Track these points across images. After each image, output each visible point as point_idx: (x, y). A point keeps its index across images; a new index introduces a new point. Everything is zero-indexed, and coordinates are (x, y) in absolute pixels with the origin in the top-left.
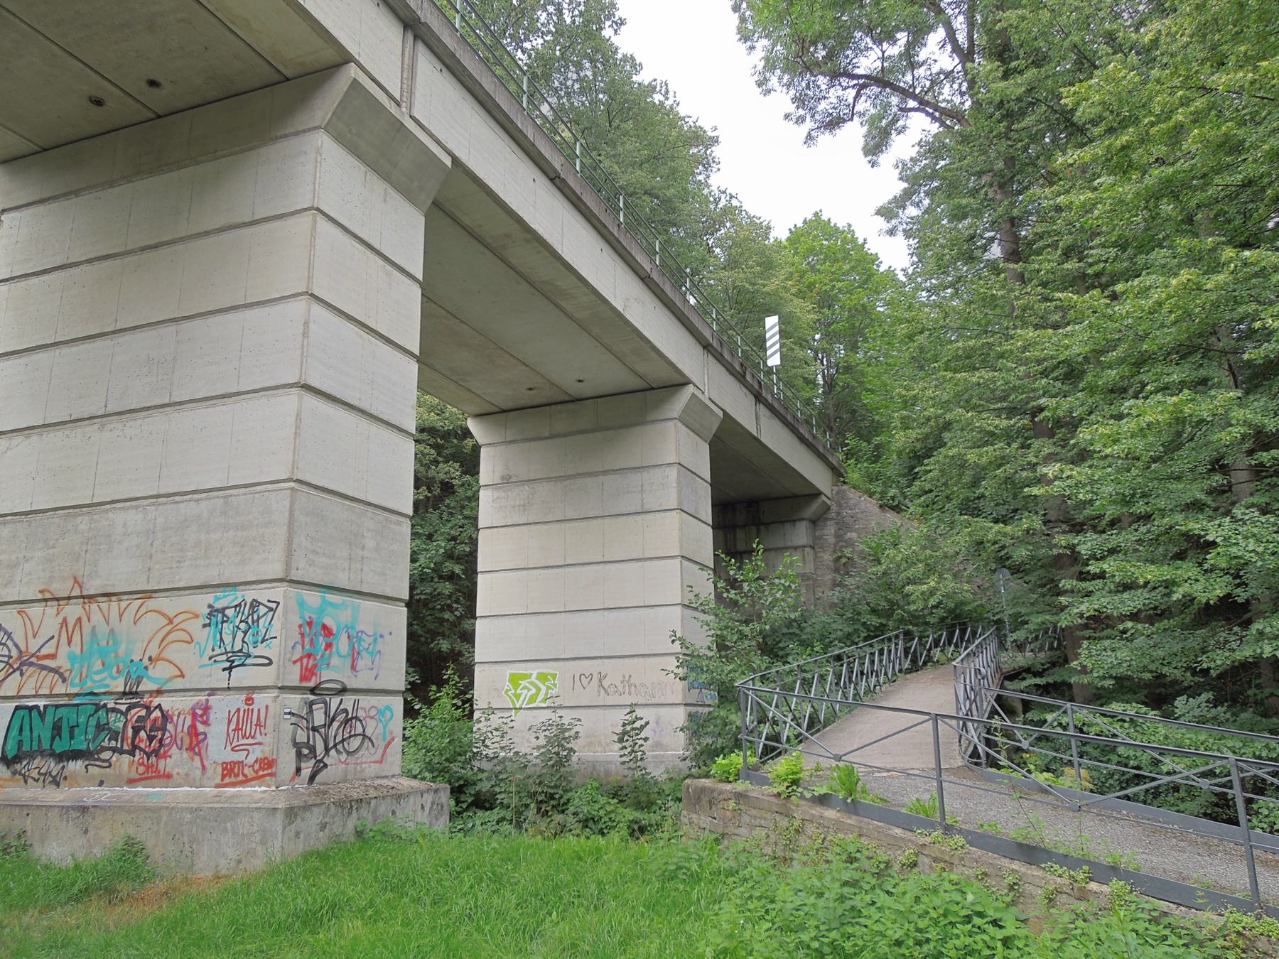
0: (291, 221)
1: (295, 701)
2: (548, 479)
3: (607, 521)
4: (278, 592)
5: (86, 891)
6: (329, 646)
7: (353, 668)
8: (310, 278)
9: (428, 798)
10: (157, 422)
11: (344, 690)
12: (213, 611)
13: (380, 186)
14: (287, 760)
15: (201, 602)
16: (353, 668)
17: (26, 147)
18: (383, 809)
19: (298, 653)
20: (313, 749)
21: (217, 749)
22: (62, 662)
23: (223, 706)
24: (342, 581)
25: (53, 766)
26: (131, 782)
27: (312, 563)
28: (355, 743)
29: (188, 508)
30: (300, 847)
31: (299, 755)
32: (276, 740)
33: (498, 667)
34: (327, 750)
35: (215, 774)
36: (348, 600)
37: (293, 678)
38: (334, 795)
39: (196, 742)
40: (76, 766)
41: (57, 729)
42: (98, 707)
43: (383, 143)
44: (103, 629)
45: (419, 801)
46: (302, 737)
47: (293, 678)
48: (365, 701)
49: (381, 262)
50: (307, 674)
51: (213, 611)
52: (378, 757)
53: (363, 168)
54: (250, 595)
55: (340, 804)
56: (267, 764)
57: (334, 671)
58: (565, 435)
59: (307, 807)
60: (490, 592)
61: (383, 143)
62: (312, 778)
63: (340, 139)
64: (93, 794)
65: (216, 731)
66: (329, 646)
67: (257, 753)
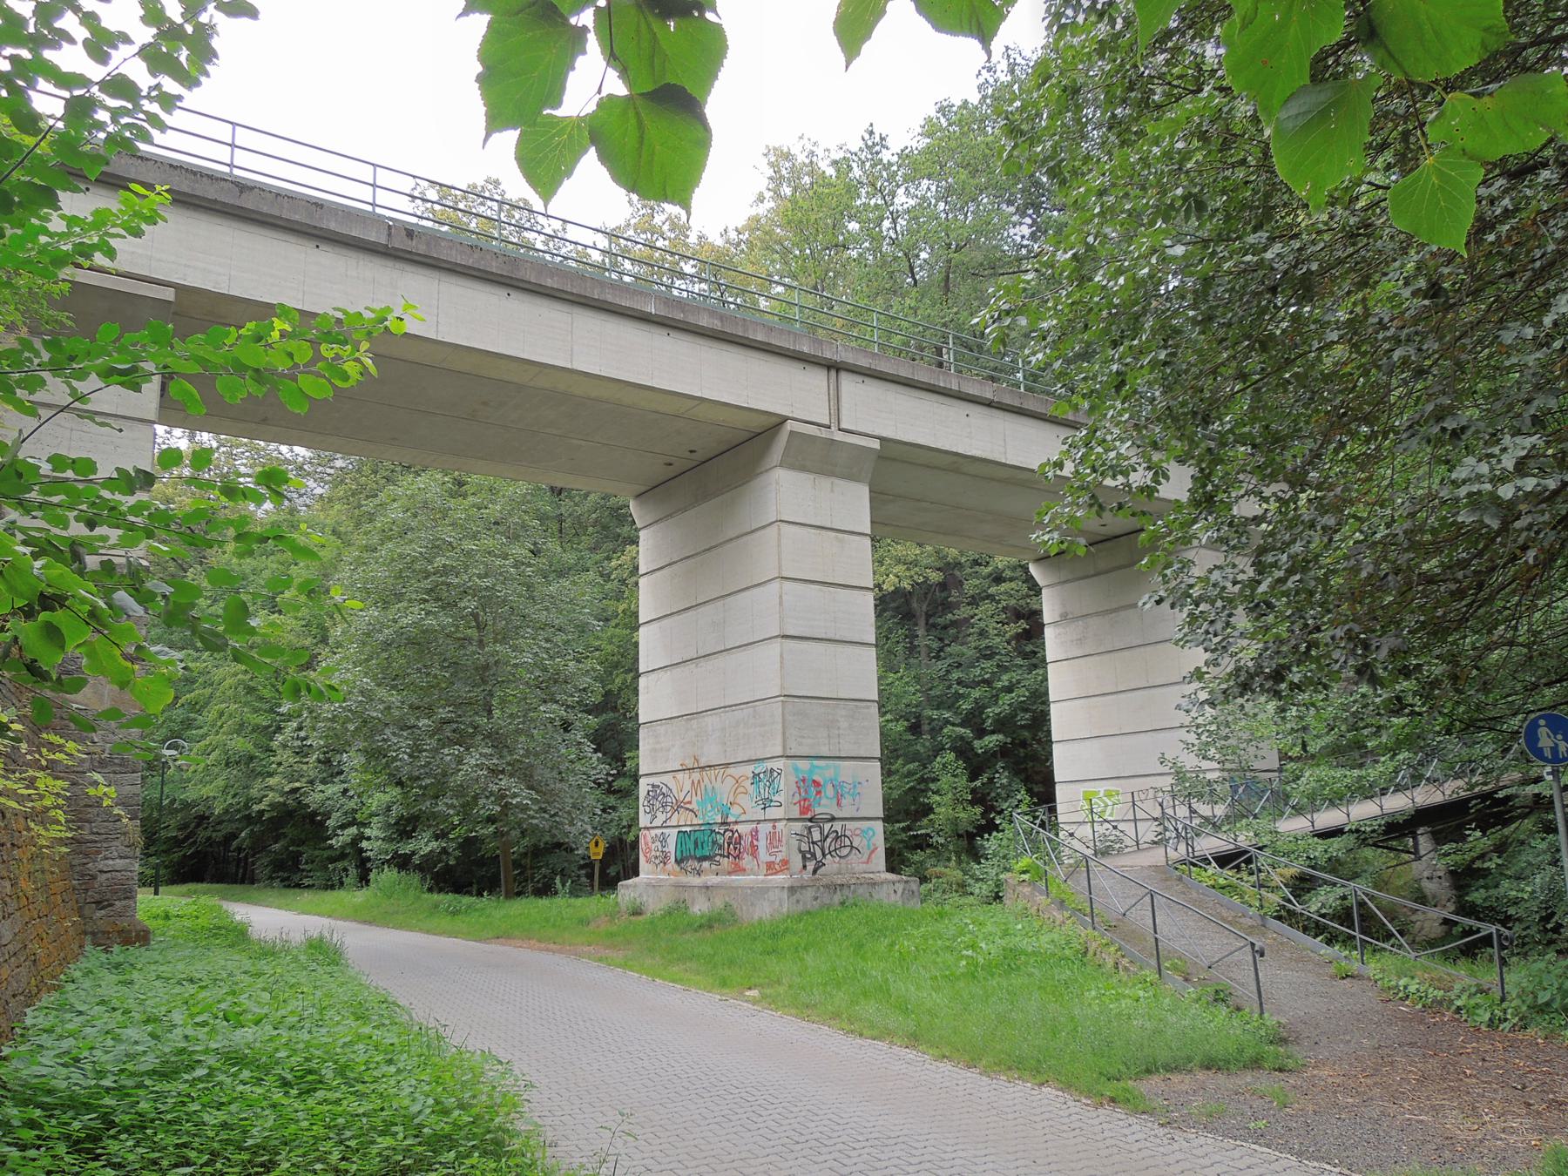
0: (768, 530)
1: (798, 827)
2: (1097, 614)
3: (1148, 648)
4: (778, 764)
5: (701, 926)
6: (819, 793)
7: (839, 804)
8: (780, 567)
9: (900, 887)
10: (719, 661)
11: (833, 819)
12: (755, 775)
13: (825, 482)
14: (797, 861)
15: (748, 770)
16: (839, 804)
17: (643, 489)
18: (861, 891)
19: (797, 798)
20: (814, 855)
21: (764, 855)
22: (693, 806)
23: (764, 829)
24: (825, 751)
25: (696, 864)
26: (729, 873)
27: (800, 744)
28: (845, 851)
29: (739, 714)
30: (800, 907)
31: (804, 857)
32: (790, 851)
33: (1072, 786)
34: (824, 855)
35: (763, 867)
36: (831, 762)
37: (796, 813)
38: (825, 881)
39: (754, 850)
40: (706, 864)
41: (696, 843)
42: (712, 831)
43: (823, 456)
44: (709, 787)
45: (891, 887)
46: (805, 847)
47: (796, 813)
48: (850, 825)
49: (833, 534)
50: (804, 810)
51: (755, 775)
52: (865, 858)
53: (812, 476)
54: (769, 765)
55: (827, 886)
56: (785, 862)
57: (824, 807)
58: (1107, 572)
59: (803, 887)
60: (1061, 721)
61: (823, 456)
62: (815, 872)
63: (792, 467)
64: (713, 880)
65: (762, 844)
66: (819, 793)
67: (780, 857)
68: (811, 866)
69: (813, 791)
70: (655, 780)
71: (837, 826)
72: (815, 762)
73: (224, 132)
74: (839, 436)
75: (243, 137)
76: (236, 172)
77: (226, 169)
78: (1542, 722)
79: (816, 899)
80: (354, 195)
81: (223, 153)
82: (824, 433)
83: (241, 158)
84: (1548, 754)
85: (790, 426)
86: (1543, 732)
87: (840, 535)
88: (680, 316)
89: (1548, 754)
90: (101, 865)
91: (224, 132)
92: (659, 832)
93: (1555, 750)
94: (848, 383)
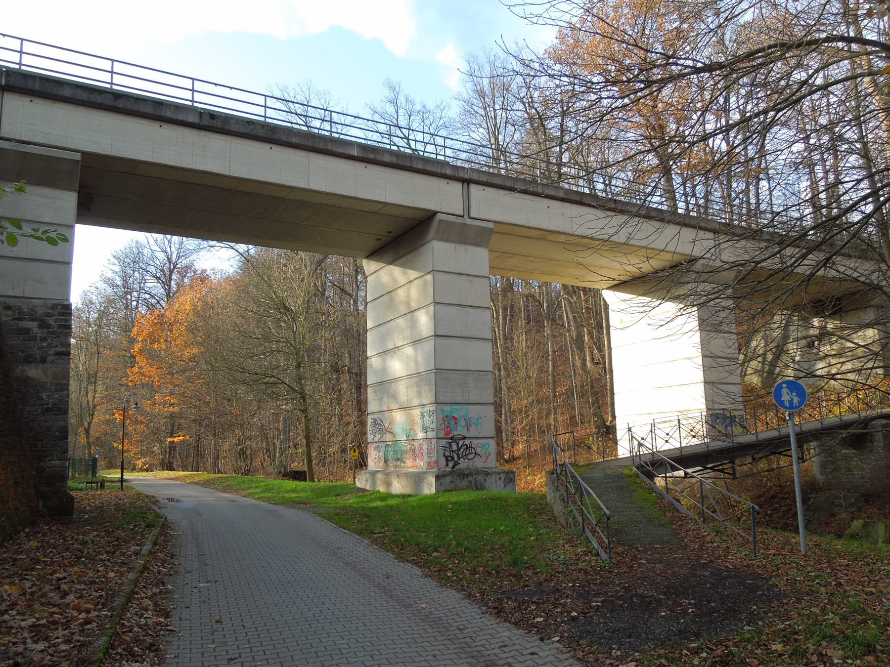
1: (444, 442)
6: (456, 423)
11: (464, 438)
13: (461, 248)
19: (443, 426)
20: (453, 458)
24: (459, 400)
28: (471, 456)
31: (447, 460)
34: (459, 458)
45: (498, 476)
46: (447, 454)
47: (442, 434)
48: (475, 442)
49: (466, 278)
52: (483, 460)
53: (453, 245)
57: (460, 431)
62: (453, 467)
63: (441, 240)
66: (456, 423)
68: (451, 464)
69: (453, 422)
70: (376, 416)
71: (467, 442)
72: (454, 407)
73: (107, 65)
74: (469, 222)
75: (118, 67)
76: (114, 87)
77: (108, 86)
78: (784, 385)
79: (452, 482)
80: (182, 96)
81: (107, 77)
82: (459, 220)
83: (117, 79)
84: (787, 404)
85: (439, 216)
86: (785, 391)
87: (471, 278)
88: (372, 156)
89: (787, 404)
90: (48, 464)
91: (107, 65)
92: (377, 445)
93: (791, 401)
94: (473, 187)
